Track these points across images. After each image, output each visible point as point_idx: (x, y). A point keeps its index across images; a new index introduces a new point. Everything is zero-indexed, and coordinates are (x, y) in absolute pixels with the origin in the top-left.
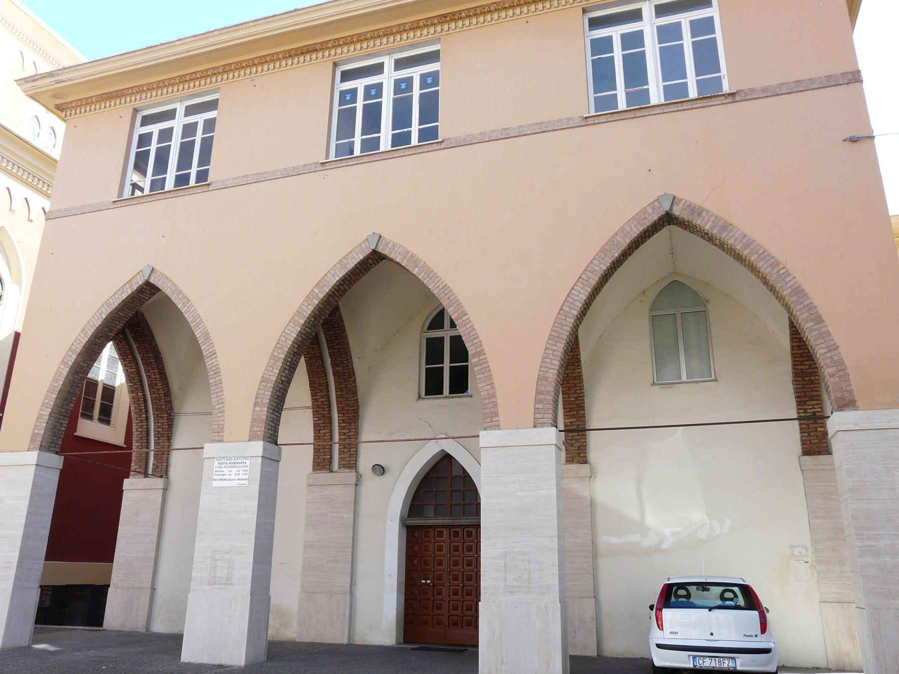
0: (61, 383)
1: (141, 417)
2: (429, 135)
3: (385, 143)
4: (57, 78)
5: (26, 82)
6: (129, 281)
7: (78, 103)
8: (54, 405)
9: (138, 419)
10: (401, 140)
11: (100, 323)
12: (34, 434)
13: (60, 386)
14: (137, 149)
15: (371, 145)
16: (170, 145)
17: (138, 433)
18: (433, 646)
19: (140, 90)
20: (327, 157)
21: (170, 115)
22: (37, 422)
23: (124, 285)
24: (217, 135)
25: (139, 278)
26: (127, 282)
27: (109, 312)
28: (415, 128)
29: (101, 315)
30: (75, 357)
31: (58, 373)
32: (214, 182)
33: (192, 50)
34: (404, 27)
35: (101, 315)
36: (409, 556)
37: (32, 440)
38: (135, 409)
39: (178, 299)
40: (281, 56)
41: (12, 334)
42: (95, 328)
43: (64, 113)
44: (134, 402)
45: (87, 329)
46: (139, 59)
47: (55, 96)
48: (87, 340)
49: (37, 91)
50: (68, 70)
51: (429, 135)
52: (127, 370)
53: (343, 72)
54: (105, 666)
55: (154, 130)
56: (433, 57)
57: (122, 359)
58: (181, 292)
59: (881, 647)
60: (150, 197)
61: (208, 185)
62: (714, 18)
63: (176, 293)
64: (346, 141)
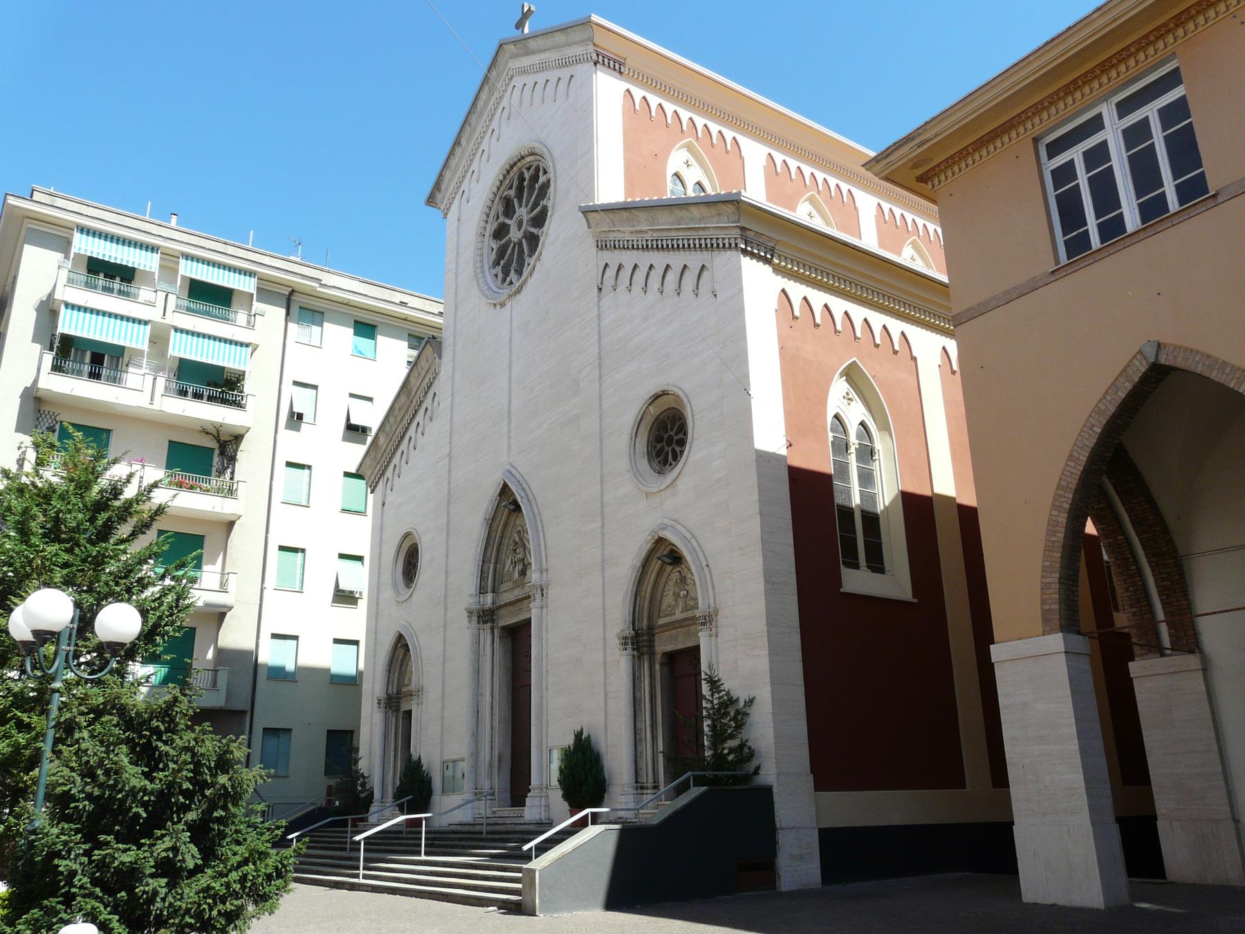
0: (1062, 535)
1: (1128, 570)
2: (1193, 190)
3: (1132, 220)
4: (918, 141)
5: (878, 162)
6: (1122, 371)
7: (948, 163)
8: (1061, 567)
10: (1153, 210)
11: (1095, 441)
12: (1044, 612)
13: (1062, 540)
14: (1055, 191)
15: (1112, 229)
16: (1078, 184)
17: (1129, 594)
18: (397, 848)
19: (1038, 108)
20: (1057, 261)
21: (1096, 124)
22: (1043, 593)
23: (1116, 379)
24: (1198, 119)
25: (1137, 363)
26: (1120, 374)
27: (1104, 422)
28: (1169, 188)
29: (1092, 429)
30: (1071, 496)
31: (1052, 523)
32: (1223, 188)
33: (1122, 16)
34: (1042, 105)
35: (1092, 429)
37: (1045, 620)
39: (1225, 376)
40: (1046, 104)
41: (897, 496)
42: (1089, 450)
43: (930, 183)
45: (1076, 455)
46: (1035, 65)
47: (915, 166)
48: (1081, 469)
49: (893, 167)
50: (933, 123)
51: (1193, 190)
53: (1048, 146)
54: (115, 809)
55: (1149, 113)
56: (1173, 79)
58: (1225, 364)
59: (242, 827)
60: (1070, 266)
61: (1214, 196)
63: (1217, 367)
64: (1075, 233)
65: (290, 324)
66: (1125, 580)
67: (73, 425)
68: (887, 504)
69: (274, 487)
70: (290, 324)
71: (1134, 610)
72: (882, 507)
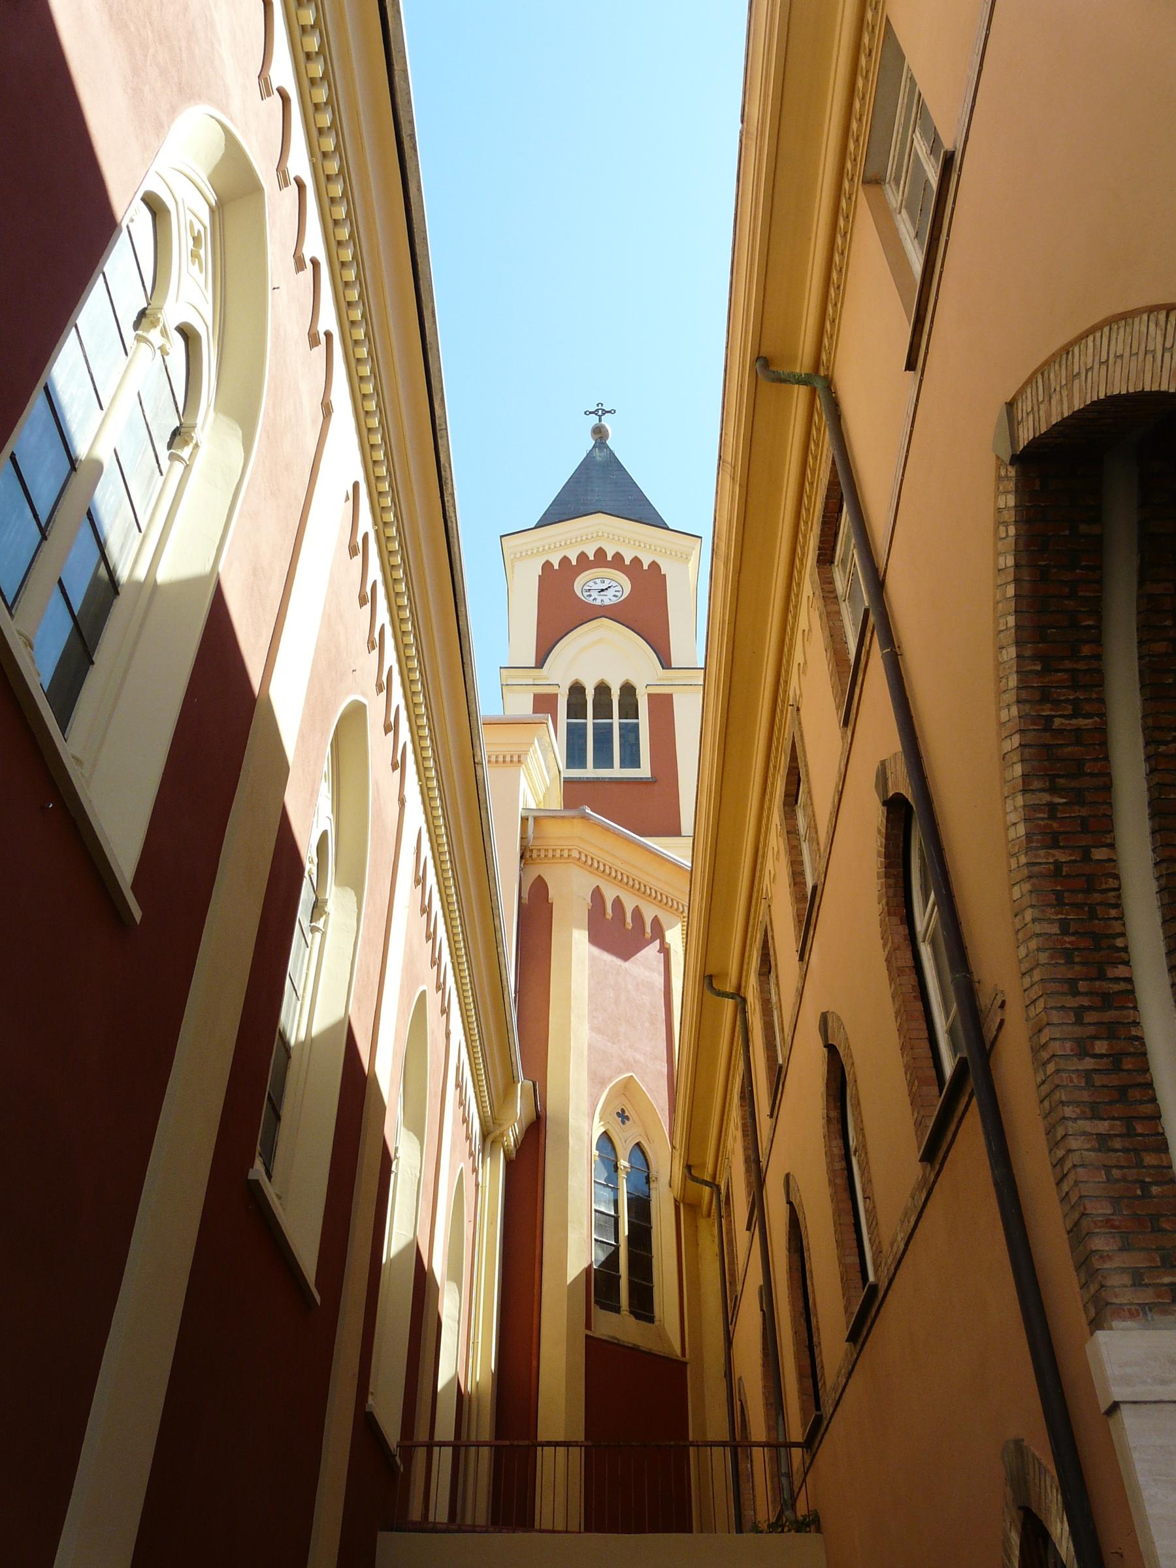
1: (1102, 976)
9: (1082, 986)
17: (1089, 1063)
36: (600, 694)
38: (1065, 931)
44: (1059, 896)
52: (1050, 718)
57: (1036, 657)
62: (519, 1536)
65: (673, 666)
66: (1079, 1012)
67: (164, 326)
68: (315, 1031)
69: (104, 284)
70: (673, 666)
71: (1103, 1127)
72: (302, 1036)
